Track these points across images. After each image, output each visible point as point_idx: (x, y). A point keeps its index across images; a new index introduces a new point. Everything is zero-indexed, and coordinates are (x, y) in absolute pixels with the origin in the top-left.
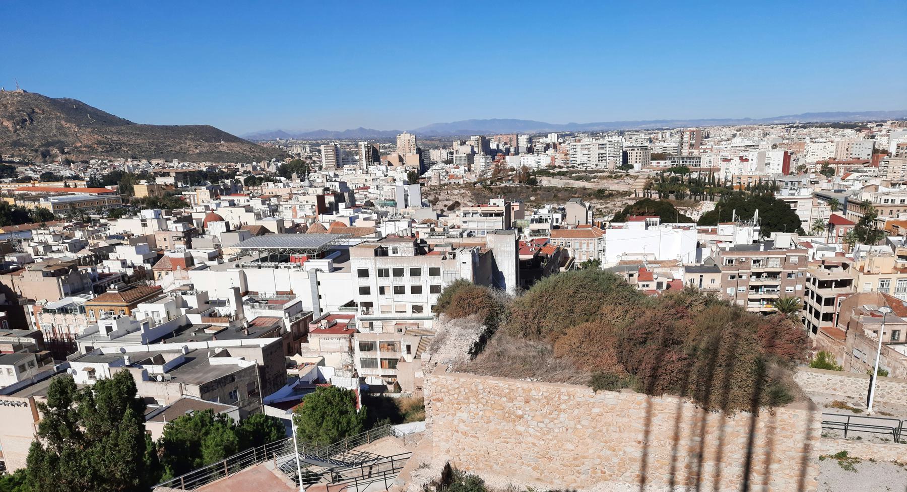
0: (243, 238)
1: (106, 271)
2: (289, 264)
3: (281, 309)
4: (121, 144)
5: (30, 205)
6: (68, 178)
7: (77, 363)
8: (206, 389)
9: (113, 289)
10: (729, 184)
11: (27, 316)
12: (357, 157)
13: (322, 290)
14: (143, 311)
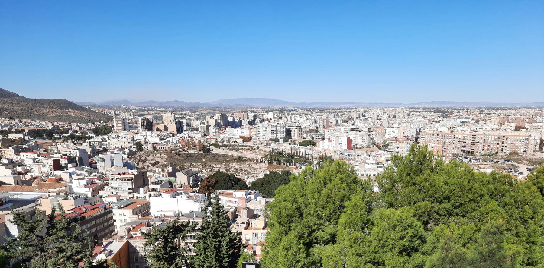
4: (3, 109)
10: (307, 156)
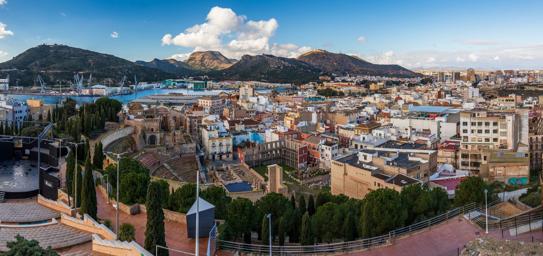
3: (427, 137)
5: (338, 90)
13: (441, 130)
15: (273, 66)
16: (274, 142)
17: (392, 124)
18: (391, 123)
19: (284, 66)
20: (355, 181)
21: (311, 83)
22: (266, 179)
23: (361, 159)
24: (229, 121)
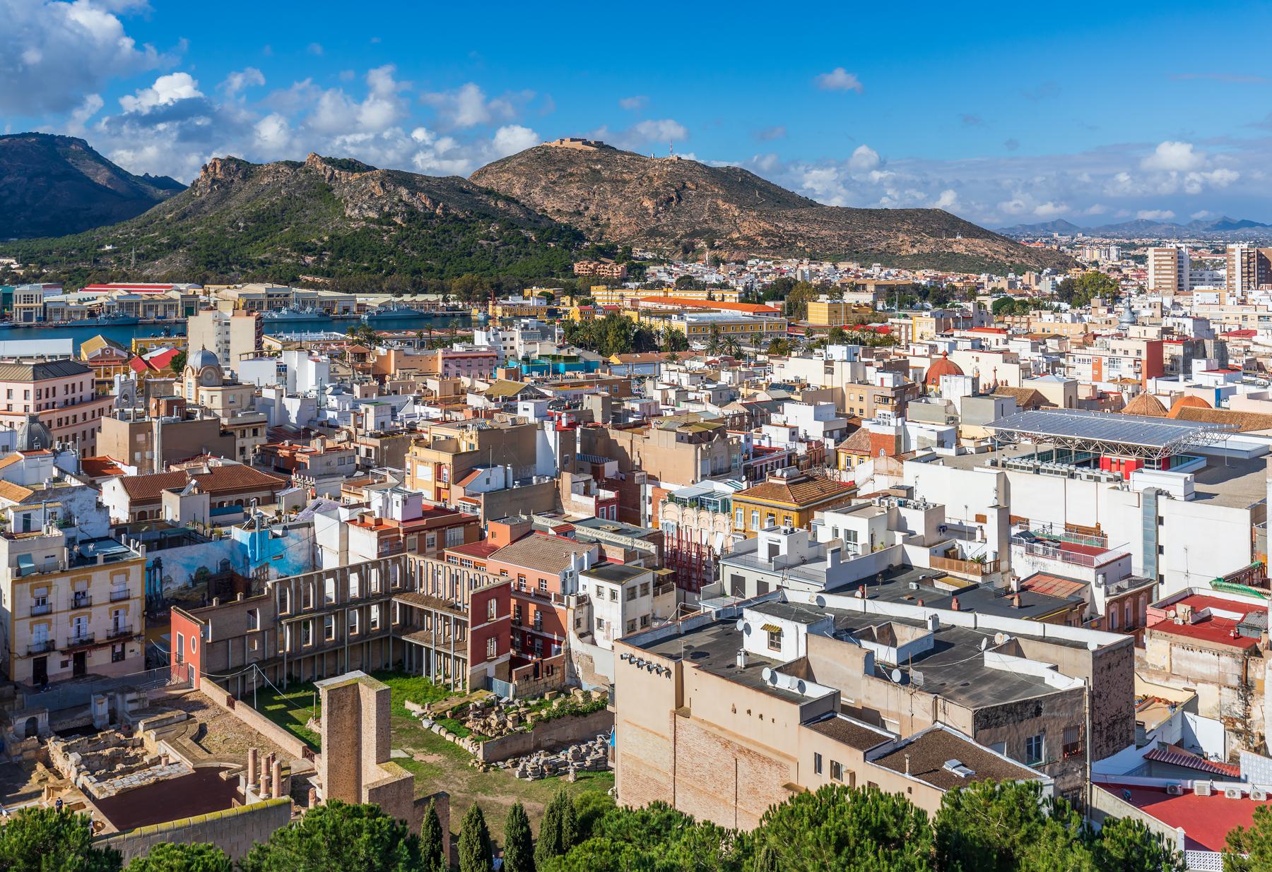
0: (1001, 411)
1: (765, 444)
2: (1097, 472)
3: (1089, 563)
5: (659, 325)
6: (714, 286)
7: (755, 613)
8: (984, 720)
9: (779, 479)
11: (642, 503)
12: (1223, 272)
14: (829, 524)
15: (357, 213)
16: (357, 568)
17: (910, 491)
18: (907, 481)
19: (412, 214)
20: (727, 744)
21: (537, 291)
22: (312, 749)
23: (756, 643)
24: (127, 483)
